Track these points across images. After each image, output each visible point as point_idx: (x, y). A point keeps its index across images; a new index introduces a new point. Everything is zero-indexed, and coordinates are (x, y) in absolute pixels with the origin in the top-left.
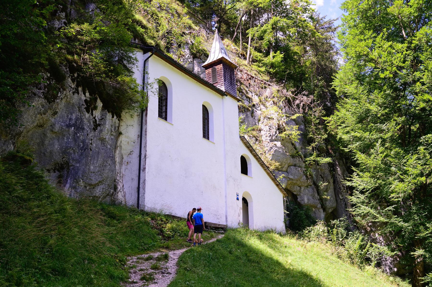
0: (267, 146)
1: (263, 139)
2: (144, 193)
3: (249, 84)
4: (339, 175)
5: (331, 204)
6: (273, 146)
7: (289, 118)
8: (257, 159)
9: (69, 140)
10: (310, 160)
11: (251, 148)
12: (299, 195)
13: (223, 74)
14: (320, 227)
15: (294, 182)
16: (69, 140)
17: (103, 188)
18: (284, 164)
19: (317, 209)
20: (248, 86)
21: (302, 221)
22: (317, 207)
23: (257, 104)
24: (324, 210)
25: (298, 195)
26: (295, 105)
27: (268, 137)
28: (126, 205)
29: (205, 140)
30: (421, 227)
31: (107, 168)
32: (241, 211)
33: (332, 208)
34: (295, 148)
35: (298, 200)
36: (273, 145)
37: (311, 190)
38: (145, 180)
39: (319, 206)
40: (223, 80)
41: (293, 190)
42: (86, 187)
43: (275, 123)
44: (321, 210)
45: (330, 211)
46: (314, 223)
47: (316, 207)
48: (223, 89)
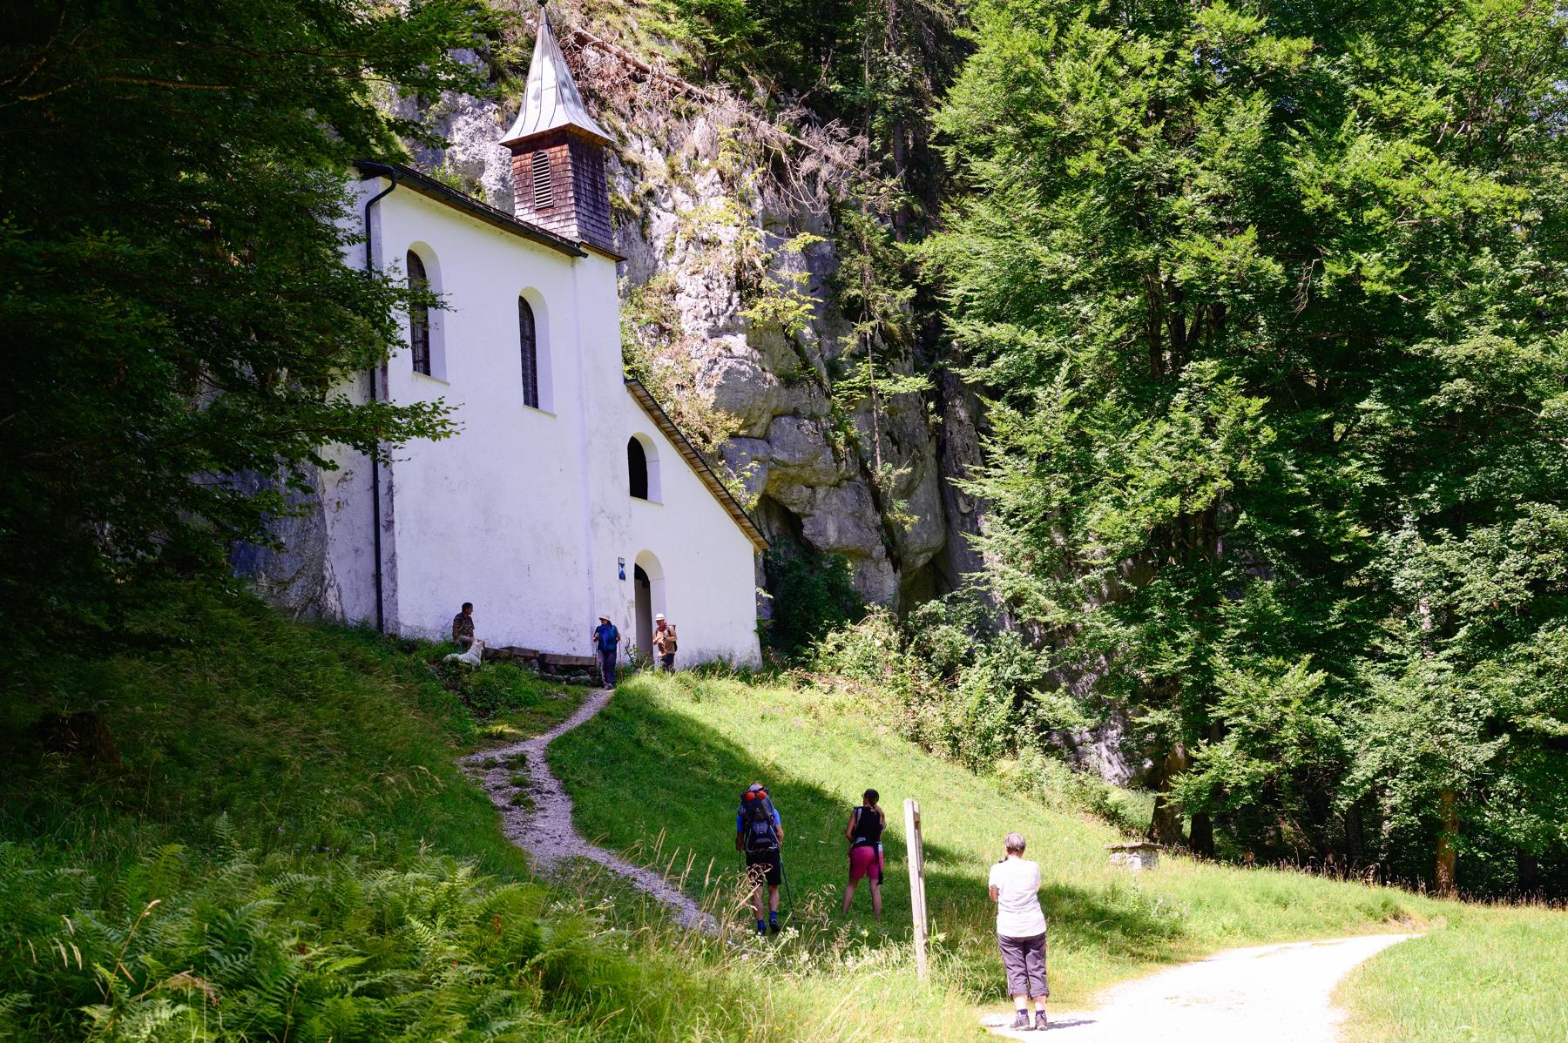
0: (699, 354)
1: (683, 326)
2: (395, 591)
3: (632, 101)
4: (960, 422)
5: (925, 536)
6: (720, 355)
7: (776, 249)
8: (675, 443)
10: (850, 389)
11: (657, 413)
12: (810, 515)
13: (570, 180)
14: (874, 632)
15: (792, 471)
17: (303, 587)
18: (757, 413)
19: (868, 563)
20: (628, 112)
21: (816, 610)
22: (868, 556)
23: (661, 187)
24: (897, 564)
25: (806, 516)
26: (800, 174)
27: (701, 321)
28: (344, 620)
29: (530, 410)
30: (1164, 645)
31: (312, 536)
32: (633, 611)
33: (927, 550)
34: (798, 348)
35: (806, 532)
36: (718, 350)
37: (849, 495)
38: (394, 554)
39: (880, 549)
40: (573, 201)
41: (785, 499)
42: (271, 589)
43: (725, 258)
44: (887, 566)
45: (921, 562)
46: (859, 615)
47: (862, 556)
48: (571, 231)
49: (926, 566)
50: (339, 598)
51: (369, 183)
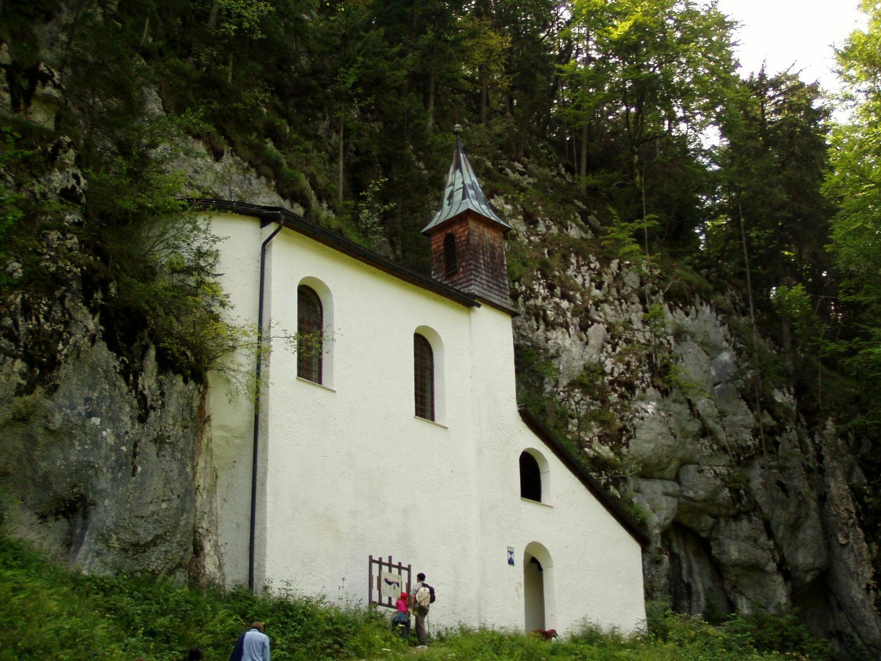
9: (86, 447)
16: (86, 447)
17: (166, 552)
24: (787, 576)
29: (422, 425)
44: (780, 579)
49: (813, 582)
50: (220, 567)
51: (266, 228)
